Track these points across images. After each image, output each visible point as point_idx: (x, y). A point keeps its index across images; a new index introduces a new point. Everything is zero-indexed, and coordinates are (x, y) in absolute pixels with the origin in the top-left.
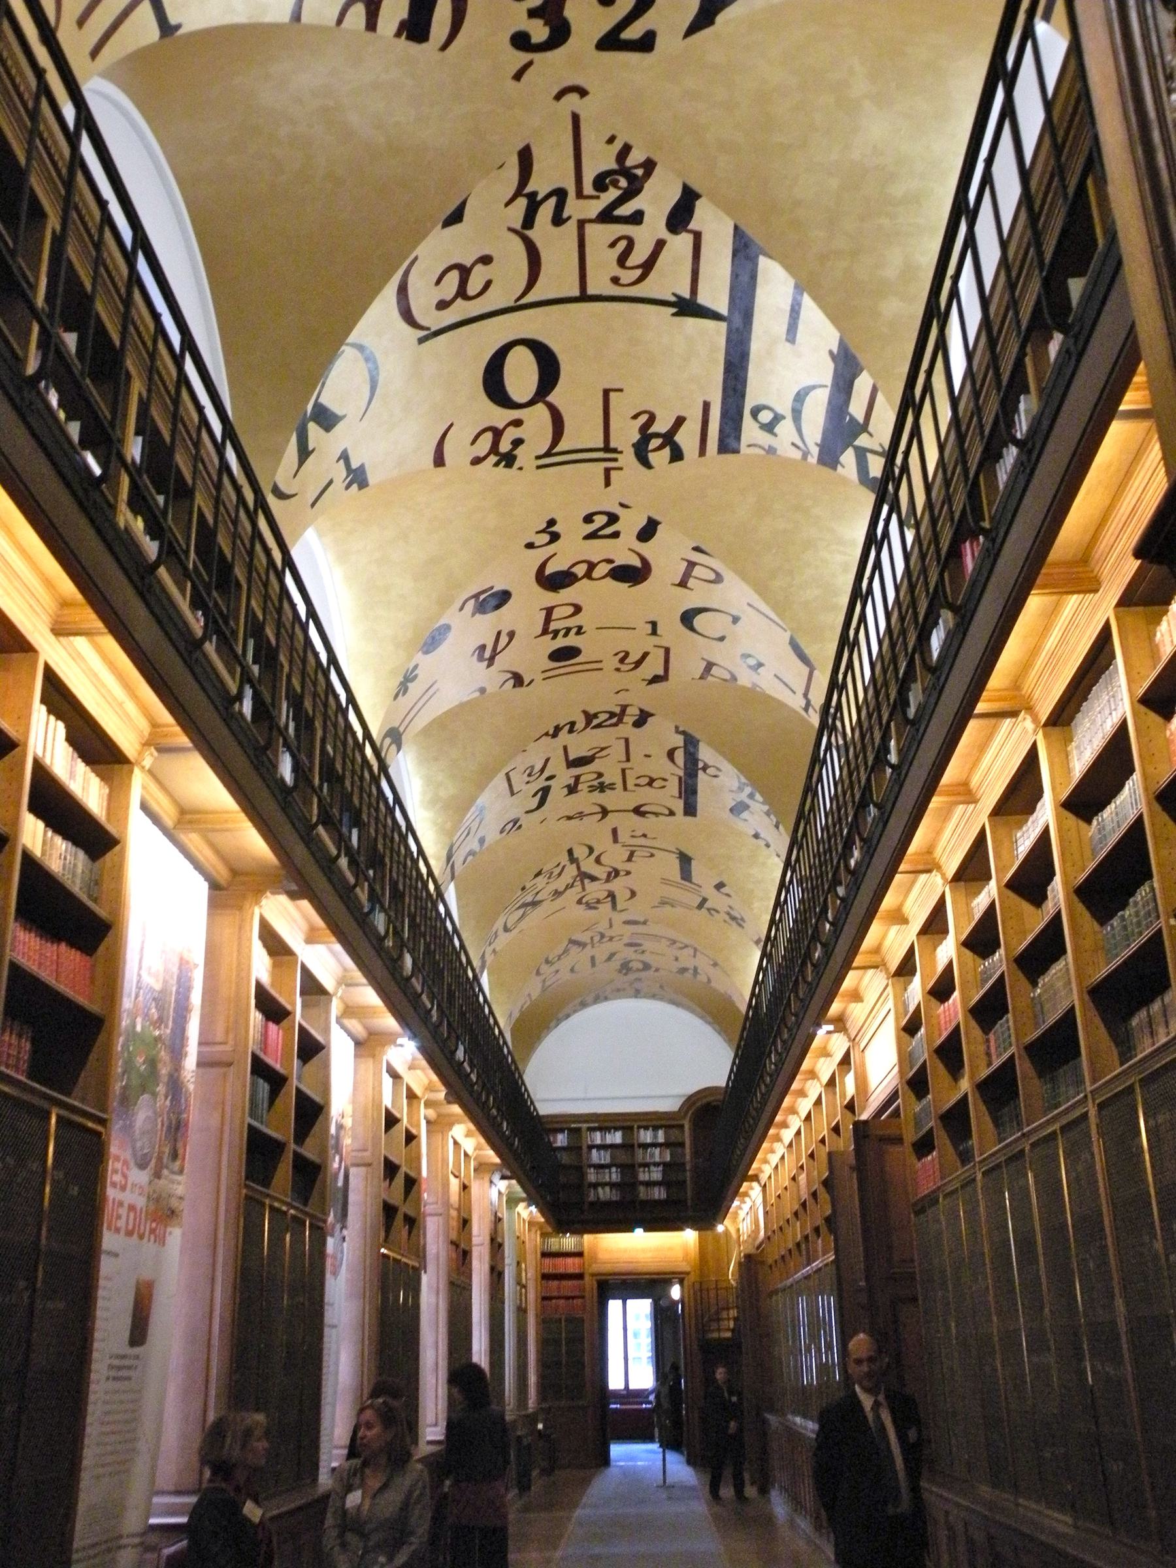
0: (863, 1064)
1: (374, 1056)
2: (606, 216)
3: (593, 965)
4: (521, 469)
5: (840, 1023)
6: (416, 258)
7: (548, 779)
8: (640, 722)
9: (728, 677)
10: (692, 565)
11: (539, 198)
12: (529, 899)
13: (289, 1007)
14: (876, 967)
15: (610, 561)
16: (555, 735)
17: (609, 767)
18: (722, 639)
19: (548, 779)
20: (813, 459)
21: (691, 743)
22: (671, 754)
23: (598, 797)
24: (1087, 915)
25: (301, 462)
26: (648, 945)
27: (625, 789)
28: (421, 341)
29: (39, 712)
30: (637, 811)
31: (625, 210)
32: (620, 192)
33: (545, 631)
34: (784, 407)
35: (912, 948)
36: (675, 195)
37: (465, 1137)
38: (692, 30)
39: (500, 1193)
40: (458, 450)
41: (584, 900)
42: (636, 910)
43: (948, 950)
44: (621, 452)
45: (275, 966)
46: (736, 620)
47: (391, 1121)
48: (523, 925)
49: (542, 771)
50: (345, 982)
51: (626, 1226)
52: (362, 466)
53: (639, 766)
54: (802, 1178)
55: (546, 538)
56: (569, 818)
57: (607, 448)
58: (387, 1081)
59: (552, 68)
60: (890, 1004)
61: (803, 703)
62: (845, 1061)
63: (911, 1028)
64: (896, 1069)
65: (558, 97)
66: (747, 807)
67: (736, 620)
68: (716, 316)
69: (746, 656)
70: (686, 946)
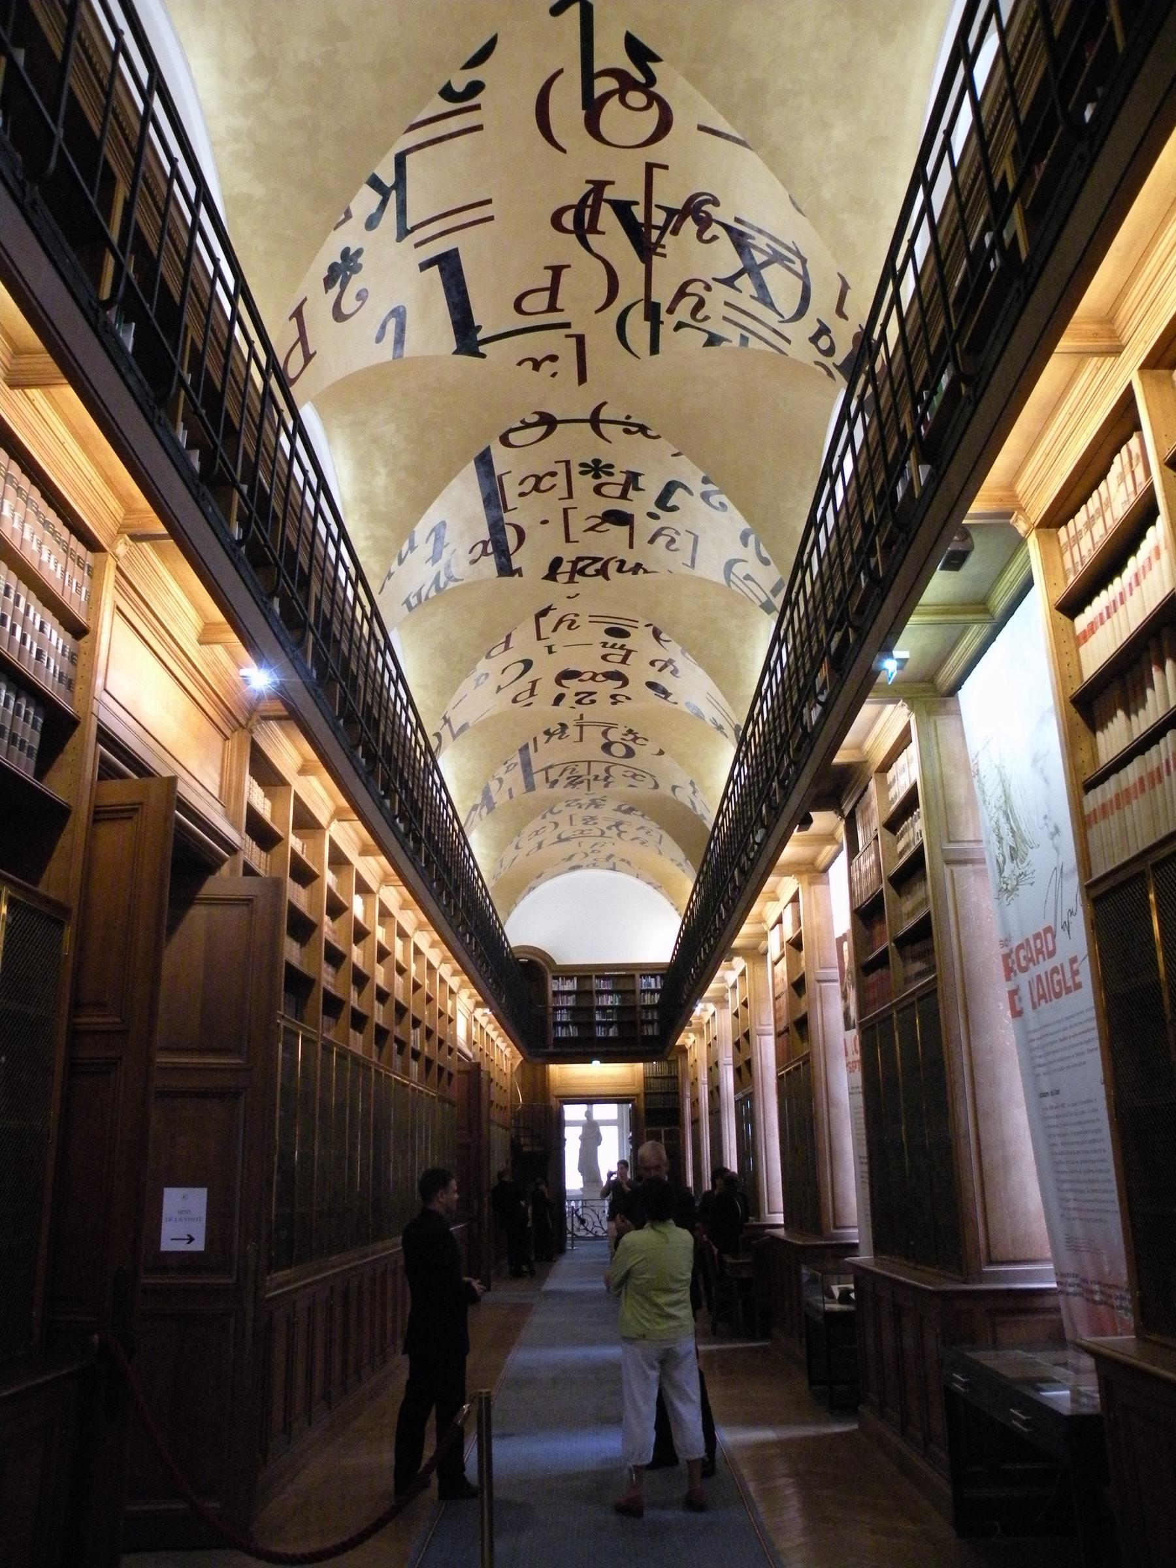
8: (556, 563)
16: (638, 566)
22: (521, 536)
27: (567, 463)
30: (548, 422)
33: (629, 652)
51: (586, 1058)
53: (551, 503)
56: (643, 429)
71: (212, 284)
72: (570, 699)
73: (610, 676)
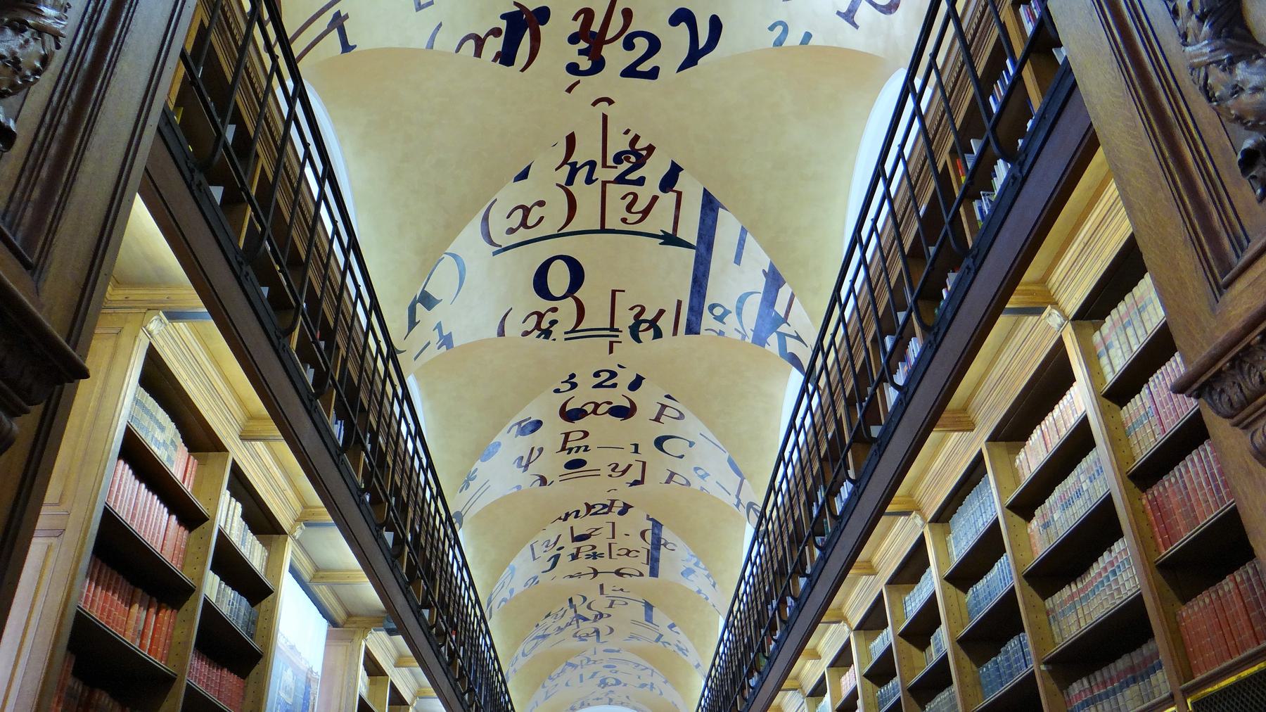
2: (621, 180)
8: (622, 513)
10: (664, 406)
12: (541, 633)
16: (565, 519)
18: (681, 457)
21: (657, 525)
22: (643, 534)
24: (967, 658)
25: (410, 329)
26: (620, 667)
28: (495, 253)
29: (225, 495)
31: (633, 176)
33: (563, 449)
34: (731, 305)
35: (823, 677)
38: (683, 67)
42: (611, 642)
43: (851, 679)
45: (371, 683)
46: (691, 444)
48: (534, 652)
50: (419, 695)
53: (620, 543)
57: (612, 329)
61: (736, 501)
65: (594, 104)
67: (691, 444)
68: (689, 246)
69: (696, 469)
71: (302, 166)
72: (625, 378)
73: (577, 414)
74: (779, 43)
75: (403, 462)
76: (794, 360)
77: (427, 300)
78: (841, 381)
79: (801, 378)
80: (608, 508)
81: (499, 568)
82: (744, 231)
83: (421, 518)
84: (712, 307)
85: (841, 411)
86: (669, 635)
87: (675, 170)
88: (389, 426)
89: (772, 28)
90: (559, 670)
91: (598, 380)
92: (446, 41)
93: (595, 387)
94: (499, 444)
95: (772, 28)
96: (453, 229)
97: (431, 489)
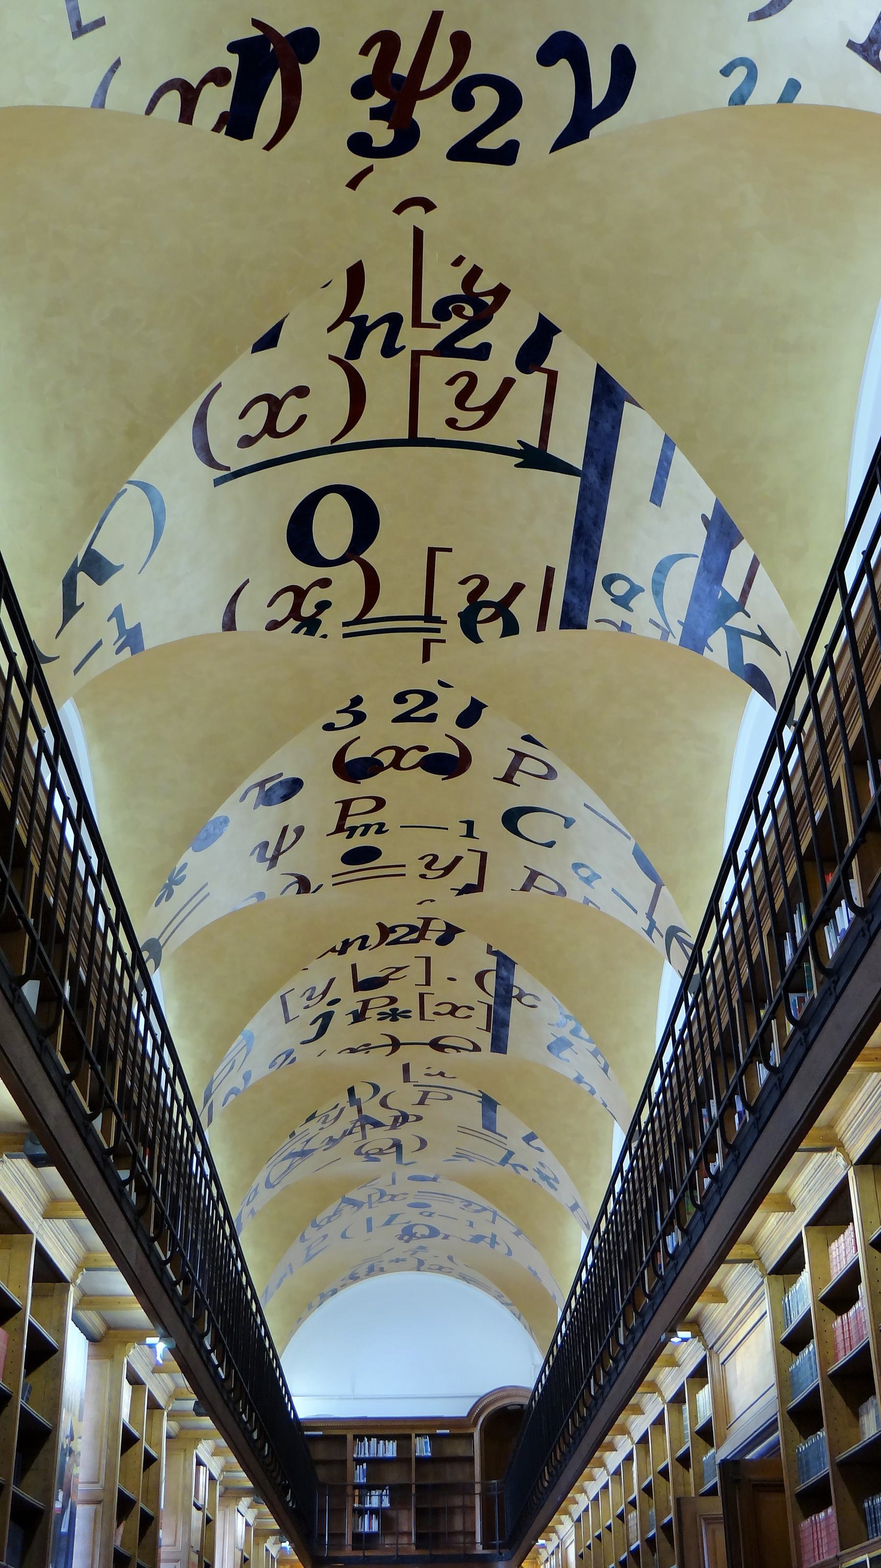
0: (724, 1380)
1: (112, 1357)
2: (446, 349)
3: (370, 1229)
4: (325, 636)
5: (697, 1327)
6: (220, 385)
7: (331, 1003)
8: (444, 941)
9: (555, 889)
10: (520, 756)
11: (368, 324)
12: (298, 1147)
13: (18, 1302)
14: (749, 1261)
15: (423, 749)
16: (342, 952)
17: (405, 992)
18: (550, 845)
19: (331, 1003)
20: (674, 640)
21: (505, 963)
22: (480, 979)
23: (389, 1027)
25: (66, 619)
26: (436, 1206)
27: (422, 1017)
28: (218, 482)
30: (436, 1045)
31: (469, 342)
32: (464, 322)
33: (340, 829)
34: (643, 578)
35: (798, 1241)
36: (530, 327)
37: (212, 1457)
38: (561, 143)
39: (211, 1478)
40: (252, 615)
41: (363, 1151)
42: (424, 1164)
44: (445, 622)
47: (129, 1440)
48: (288, 1180)
49: (324, 994)
50: (86, 1265)
52: (138, 628)
53: (440, 992)
54: (633, 1517)
55: (349, 718)
56: (352, 1051)
57: (428, 616)
58: (127, 1390)
59: (396, 176)
60: (765, 1305)
61: (646, 924)
62: (700, 1374)
63: (795, 1341)
64: (774, 1392)
65: (399, 210)
66: (569, 1045)
68: (566, 469)
69: (577, 866)
70: (485, 1209)
72: (449, 706)
74: (739, 98)
75: (59, 862)
76: (757, 679)
77: (96, 566)
78: (841, 720)
79: (771, 715)
80: (419, 932)
81: (223, 1037)
82: (669, 444)
83: (91, 959)
84: (609, 580)
85: (839, 773)
86: (524, 1154)
87: (545, 332)
88: (33, 799)
89: (726, 72)
90: (330, 1210)
91: (403, 709)
92: (130, 94)
93: (395, 720)
94: (226, 821)
95: (726, 72)
96: (142, 438)
97: (106, 911)
